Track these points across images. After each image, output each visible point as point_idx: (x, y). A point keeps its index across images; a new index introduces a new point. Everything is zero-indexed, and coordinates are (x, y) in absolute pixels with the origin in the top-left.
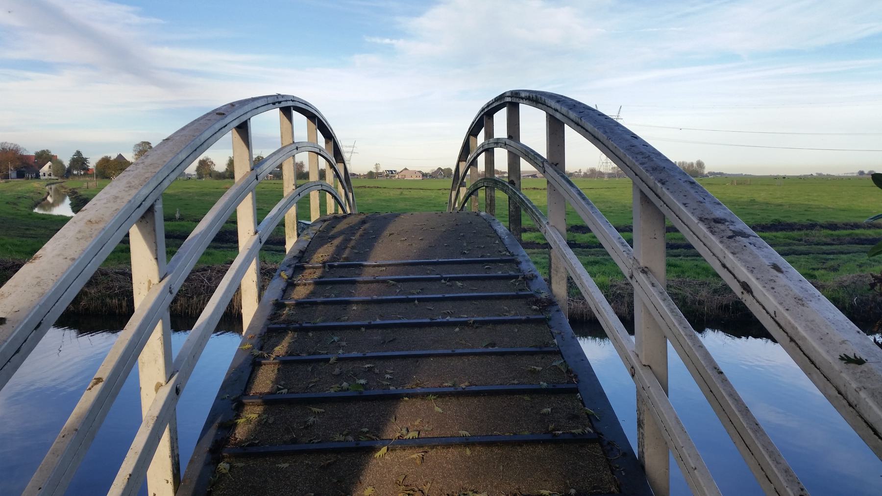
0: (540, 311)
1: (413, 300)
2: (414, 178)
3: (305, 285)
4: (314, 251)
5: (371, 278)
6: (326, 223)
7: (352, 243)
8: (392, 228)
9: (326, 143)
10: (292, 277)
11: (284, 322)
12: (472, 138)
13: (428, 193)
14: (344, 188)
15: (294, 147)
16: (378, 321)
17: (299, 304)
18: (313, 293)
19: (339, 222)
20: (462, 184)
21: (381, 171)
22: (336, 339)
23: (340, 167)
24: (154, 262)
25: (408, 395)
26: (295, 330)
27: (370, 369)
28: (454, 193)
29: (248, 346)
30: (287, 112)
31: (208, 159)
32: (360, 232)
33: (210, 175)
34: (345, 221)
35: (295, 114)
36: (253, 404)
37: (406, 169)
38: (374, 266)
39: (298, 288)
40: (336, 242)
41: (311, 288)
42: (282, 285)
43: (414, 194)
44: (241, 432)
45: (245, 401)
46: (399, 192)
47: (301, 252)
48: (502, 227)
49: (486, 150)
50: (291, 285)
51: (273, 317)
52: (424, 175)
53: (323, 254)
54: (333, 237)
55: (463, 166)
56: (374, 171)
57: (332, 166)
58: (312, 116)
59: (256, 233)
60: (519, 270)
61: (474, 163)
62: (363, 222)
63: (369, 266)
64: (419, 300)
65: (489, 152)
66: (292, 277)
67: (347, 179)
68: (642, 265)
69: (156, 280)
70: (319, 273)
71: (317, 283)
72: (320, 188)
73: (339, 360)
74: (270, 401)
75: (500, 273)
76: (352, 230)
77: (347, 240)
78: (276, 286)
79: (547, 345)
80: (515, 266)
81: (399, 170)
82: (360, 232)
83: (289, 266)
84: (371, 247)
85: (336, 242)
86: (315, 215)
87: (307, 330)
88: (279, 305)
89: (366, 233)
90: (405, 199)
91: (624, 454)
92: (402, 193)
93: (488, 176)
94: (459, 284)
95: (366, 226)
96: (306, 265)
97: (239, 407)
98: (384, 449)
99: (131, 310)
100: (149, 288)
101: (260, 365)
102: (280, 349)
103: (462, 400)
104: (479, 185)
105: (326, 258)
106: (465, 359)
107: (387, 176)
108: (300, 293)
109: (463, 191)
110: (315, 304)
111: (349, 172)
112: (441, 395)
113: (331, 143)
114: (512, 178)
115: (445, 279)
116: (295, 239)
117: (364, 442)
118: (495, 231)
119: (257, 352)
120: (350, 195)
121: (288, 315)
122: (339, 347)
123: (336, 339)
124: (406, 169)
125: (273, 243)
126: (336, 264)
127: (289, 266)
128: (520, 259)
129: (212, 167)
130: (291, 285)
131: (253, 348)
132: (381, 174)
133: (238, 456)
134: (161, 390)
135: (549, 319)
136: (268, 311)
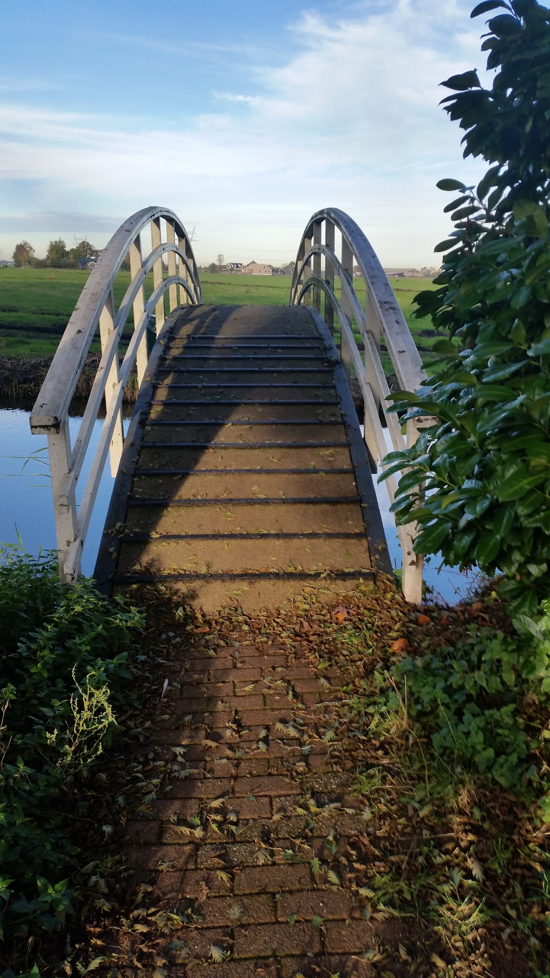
0: (329, 367)
1: (249, 358)
2: (263, 273)
3: (177, 348)
4: (180, 328)
5: (222, 346)
6: (185, 310)
7: (206, 324)
8: (234, 315)
9: (180, 241)
10: (168, 343)
11: (167, 367)
12: (306, 240)
13: (277, 292)
14: (193, 282)
15: (162, 248)
16: (226, 369)
17: (175, 359)
18: (183, 353)
19: (194, 310)
20: (299, 282)
21: (224, 263)
22: (201, 377)
23: (190, 262)
24: (111, 318)
25: (243, 403)
26: (175, 372)
27: (222, 392)
28: (293, 290)
29: (148, 379)
30: (157, 221)
31: (26, 244)
32: (212, 317)
33: (30, 263)
34: (199, 309)
35: (163, 221)
36: (158, 405)
37: (253, 262)
38: (224, 339)
39: (173, 350)
40: (195, 322)
41: (181, 350)
42: (162, 348)
43: (262, 292)
44: (153, 415)
45: (153, 403)
46: (244, 289)
47: (170, 328)
48: (322, 316)
49: (314, 253)
50: (167, 348)
51: (160, 365)
52: (275, 271)
53: (186, 330)
54: (192, 320)
55: (300, 264)
56: (217, 263)
57: (184, 262)
58: (171, 220)
59: (145, 311)
60: (322, 344)
61: (307, 263)
62: (214, 310)
63: (220, 338)
64: (253, 358)
65: (317, 255)
66: (168, 343)
67: (195, 273)
68: (368, 328)
69: (112, 328)
70: (185, 342)
71: (185, 347)
72: (177, 281)
73: (204, 387)
74: (165, 404)
75: (308, 345)
76: (205, 315)
77: (203, 322)
78: (158, 350)
79: (328, 383)
80: (320, 341)
81: (245, 263)
82: (212, 317)
83: (164, 337)
84: (221, 327)
85: (195, 322)
86: (173, 306)
87: (183, 372)
88: (162, 359)
89: (216, 318)
90: (251, 298)
91: (355, 430)
92: (248, 291)
93: (316, 276)
94: (280, 351)
95: (216, 313)
96: (176, 337)
97: (150, 405)
98: (230, 424)
99: (133, 330)
100: (109, 333)
101: (157, 388)
102: (168, 381)
103: (274, 407)
104: (310, 283)
105: (189, 333)
106: (278, 389)
107: (232, 269)
108: (175, 352)
109: (300, 288)
110: (186, 358)
111: (198, 265)
112: (261, 404)
113: (184, 241)
114: (329, 279)
115: (271, 347)
116: (163, 322)
117: (220, 421)
118: (313, 319)
119: (154, 382)
120: (198, 289)
121: (169, 364)
122: (204, 381)
123: (201, 377)
124: (253, 262)
125: (151, 323)
126: (196, 336)
127: (164, 337)
128: (325, 337)
129: (31, 253)
130: (167, 348)
131: (151, 380)
132: (224, 267)
133: (154, 425)
134: (116, 386)
135: (334, 371)
136: (156, 362)
